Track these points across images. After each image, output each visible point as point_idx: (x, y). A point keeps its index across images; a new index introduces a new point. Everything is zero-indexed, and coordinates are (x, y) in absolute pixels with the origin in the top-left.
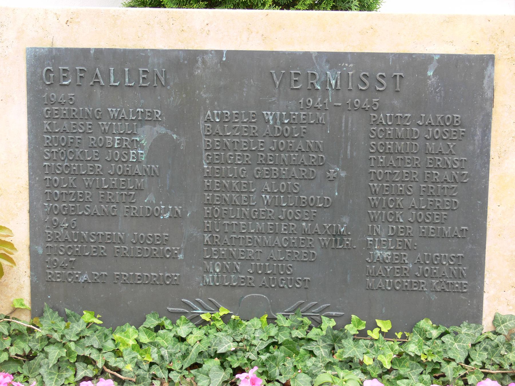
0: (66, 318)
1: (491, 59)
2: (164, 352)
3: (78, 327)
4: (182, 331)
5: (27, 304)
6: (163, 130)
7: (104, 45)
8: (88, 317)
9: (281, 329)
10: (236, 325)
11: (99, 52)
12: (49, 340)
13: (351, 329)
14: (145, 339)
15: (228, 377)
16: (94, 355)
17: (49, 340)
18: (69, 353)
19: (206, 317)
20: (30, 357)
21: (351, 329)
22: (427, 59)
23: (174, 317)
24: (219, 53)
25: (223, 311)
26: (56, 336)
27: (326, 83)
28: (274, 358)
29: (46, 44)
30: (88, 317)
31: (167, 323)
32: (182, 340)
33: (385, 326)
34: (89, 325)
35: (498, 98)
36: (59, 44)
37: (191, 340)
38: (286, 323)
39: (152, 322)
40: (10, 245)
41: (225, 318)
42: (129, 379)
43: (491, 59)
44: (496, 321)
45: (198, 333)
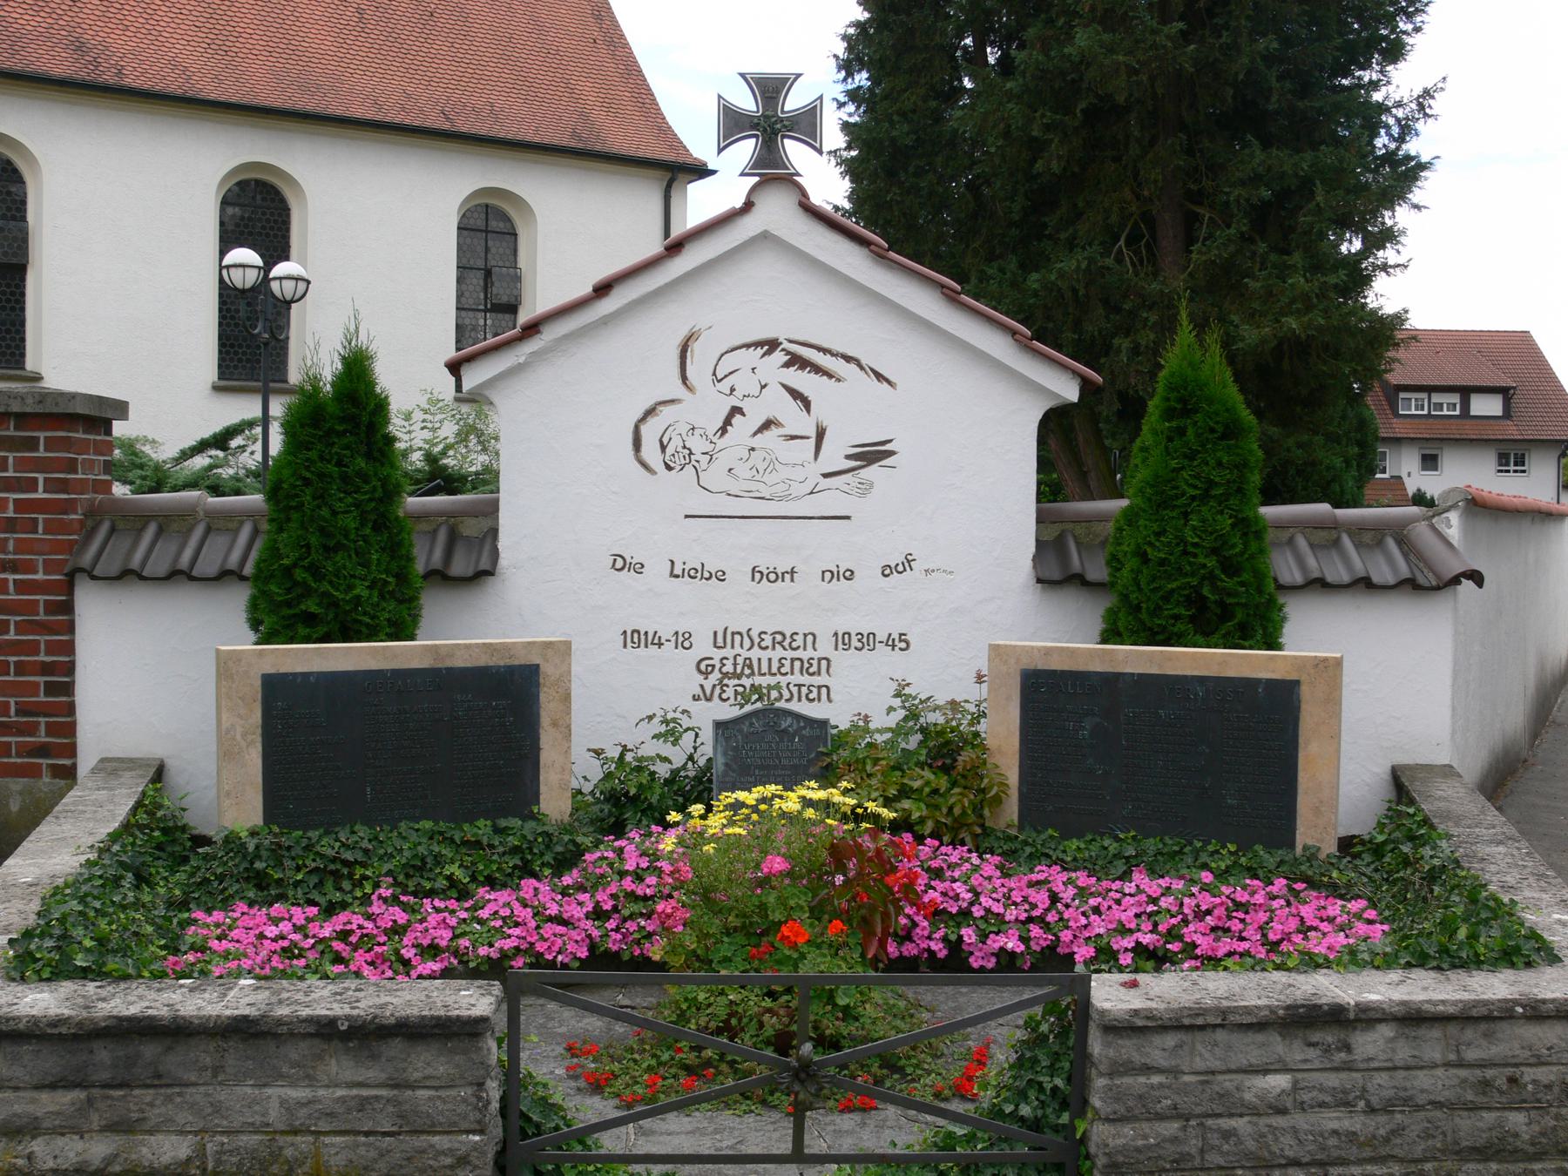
0: (1039, 832)
1: (1297, 683)
2: (1093, 854)
3: (1043, 837)
4: (1106, 843)
5: (1016, 822)
6: (1098, 720)
7: (1066, 668)
8: (1050, 831)
9: (1164, 844)
10: (1140, 841)
11: (1063, 672)
12: (1026, 843)
13: (1211, 848)
14: (1082, 846)
15: (1404, 146)
16: (1051, 853)
17: (1026, 843)
18: (1037, 850)
19: (1122, 836)
20: (1014, 852)
21: (1211, 848)
22: (1258, 681)
23: (1102, 835)
24: (1133, 674)
25: (1133, 833)
26: (1030, 840)
27: (1196, 694)
28: (1157, 861)
29: (1032, 667)
30: (1050, 831)
31: (1098, 839)
32: (1106, 848)
33: (1232, 848)
34: (1051, 837)
35: (1304, 706)
36: (1040, 667)
37: (1110, 848)
38: (1170, 842)
39: (1089, 837)
40: (1007, 785)
41: (1134, 838)
42: (21, 1094)
43: (1297, 683)
44: (1305, 848)
45: (1115, 845)
